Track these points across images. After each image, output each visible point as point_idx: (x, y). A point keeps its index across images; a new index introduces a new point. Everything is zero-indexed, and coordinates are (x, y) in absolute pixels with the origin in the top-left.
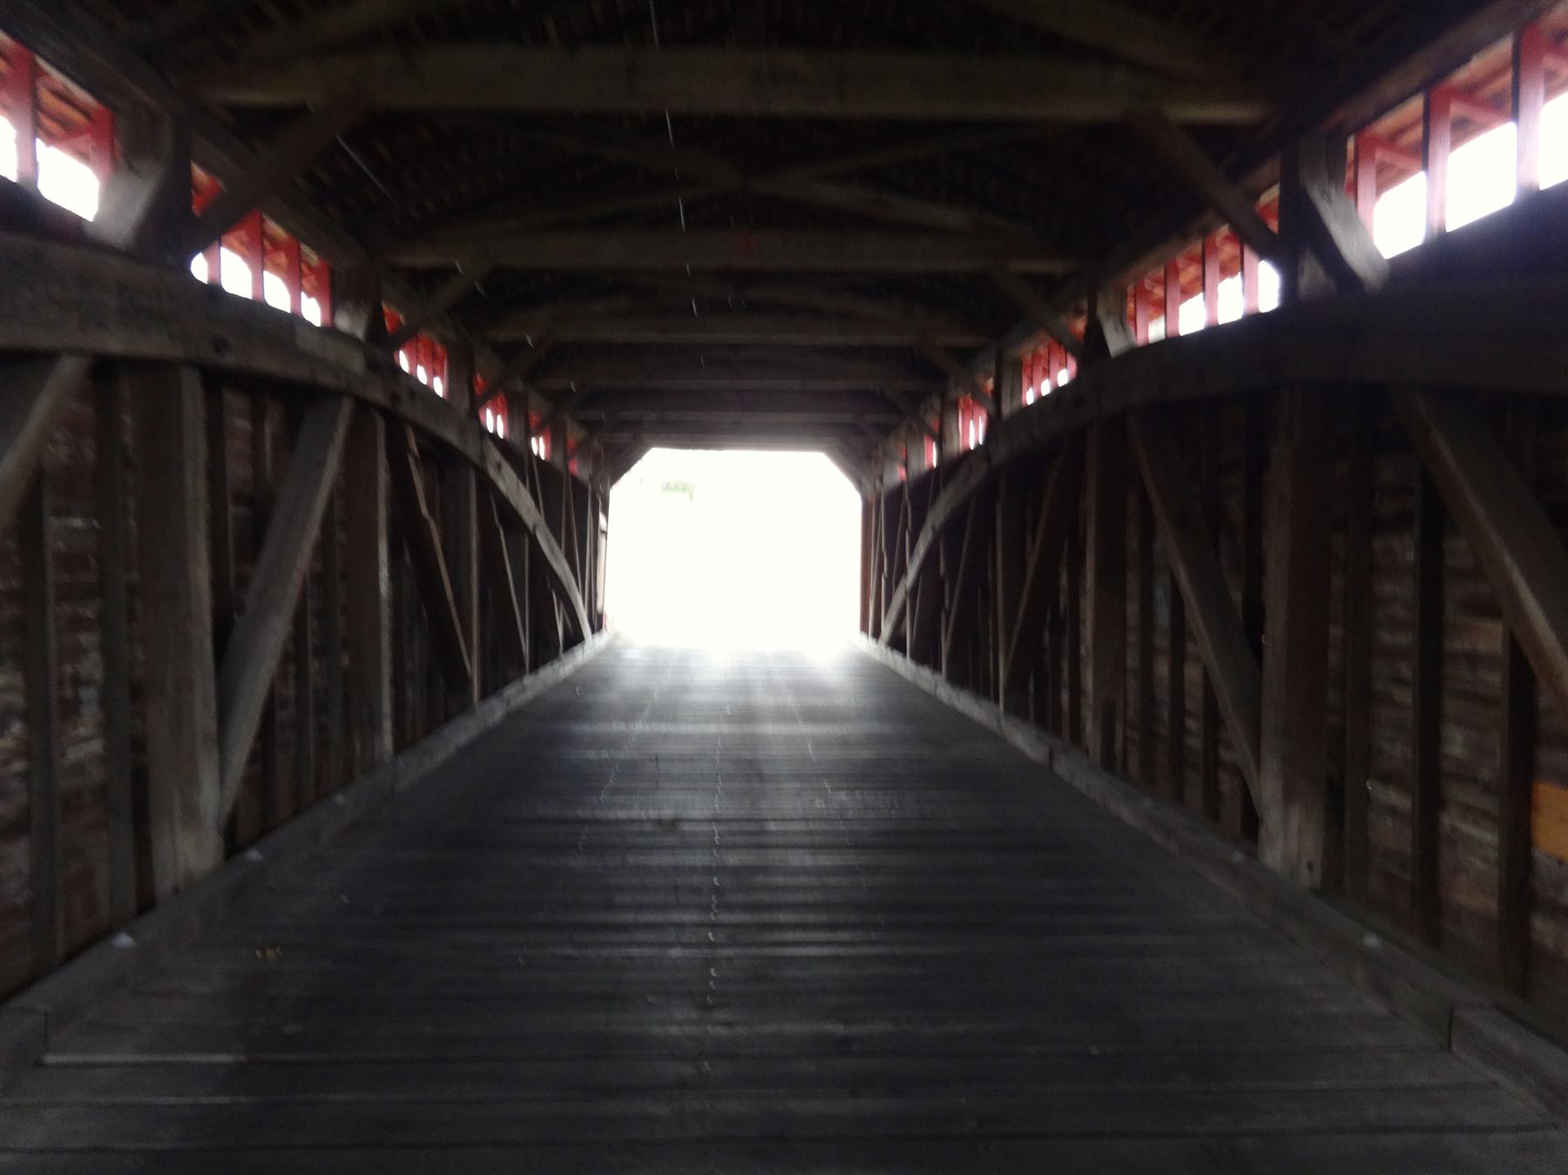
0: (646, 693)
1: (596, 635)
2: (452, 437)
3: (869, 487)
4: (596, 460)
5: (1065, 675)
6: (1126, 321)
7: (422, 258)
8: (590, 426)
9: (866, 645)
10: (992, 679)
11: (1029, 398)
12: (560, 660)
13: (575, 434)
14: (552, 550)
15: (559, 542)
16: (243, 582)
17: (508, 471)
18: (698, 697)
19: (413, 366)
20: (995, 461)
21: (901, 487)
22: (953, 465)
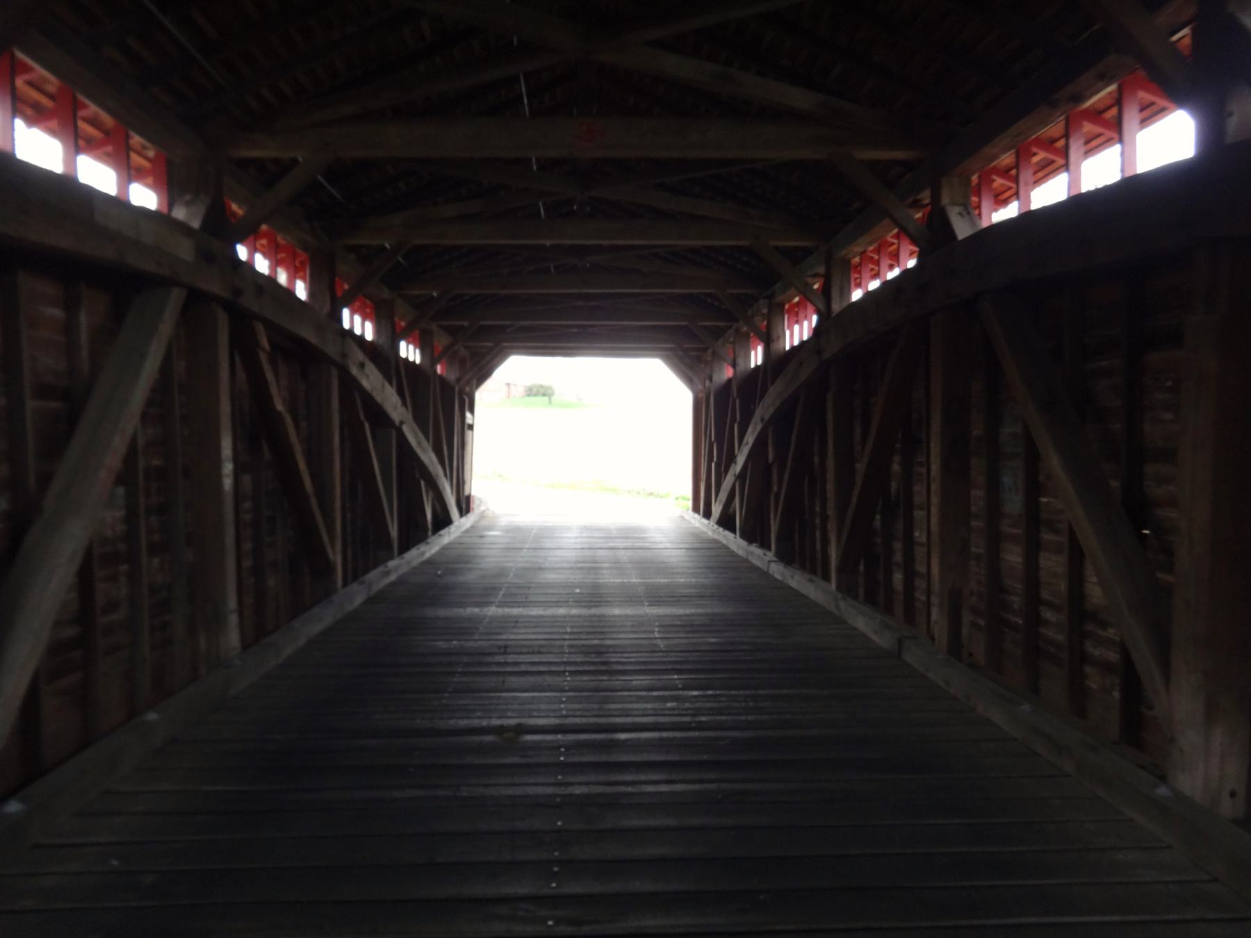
0: (502, 572)
2: (307, 333)
3: (700, 387)
4: (463, 362)
5: (898, 557)
6: (972, 211)
7: (264, 150)
8: (453, 332)
9: (697, 522)
10: (819, 555)
11: (857, 295)
12: (429, 540)
13: (441, 341)
14: (419, 444)
15: (427, 438)
16: (45, 480)
17: (371, 368)
18: (551, 577)
19: (292, 280)
20: (827, 355)
21: (730, 381)
22: (778, 363)
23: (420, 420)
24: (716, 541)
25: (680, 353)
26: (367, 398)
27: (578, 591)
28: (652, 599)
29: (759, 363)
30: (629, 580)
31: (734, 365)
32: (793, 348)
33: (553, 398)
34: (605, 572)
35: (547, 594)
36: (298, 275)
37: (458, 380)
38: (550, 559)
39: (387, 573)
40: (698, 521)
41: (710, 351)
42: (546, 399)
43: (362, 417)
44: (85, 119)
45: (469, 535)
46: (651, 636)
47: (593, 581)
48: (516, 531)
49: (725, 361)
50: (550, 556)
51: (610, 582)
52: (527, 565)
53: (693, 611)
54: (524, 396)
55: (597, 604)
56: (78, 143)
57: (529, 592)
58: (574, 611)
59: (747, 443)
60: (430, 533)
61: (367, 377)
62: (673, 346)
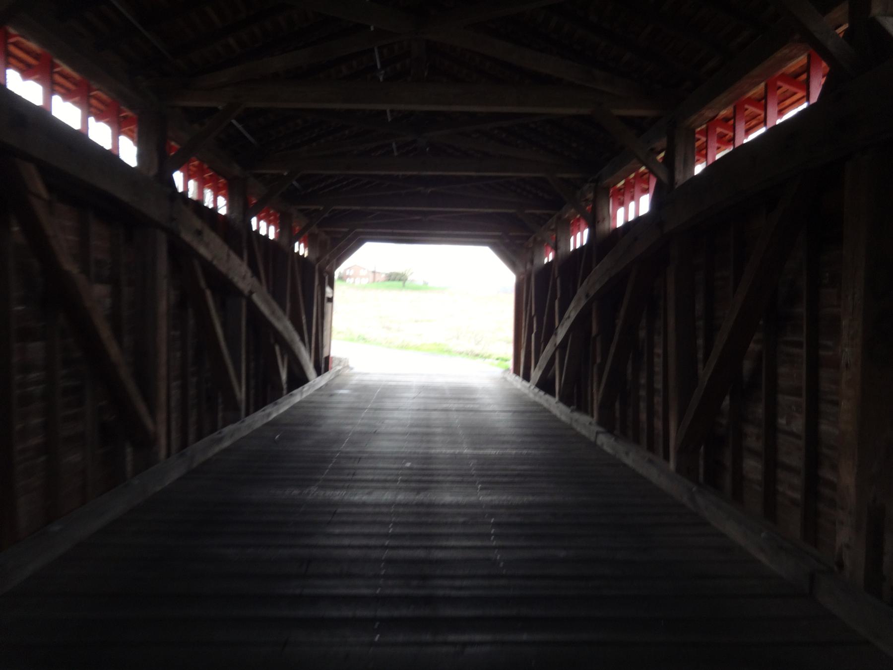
1: (320, 378)
11: (699, 169)
14: (273, 313)
18: (384, 445)
23: (277, 295)
24: (535, 404)
25: (507, 241)
26: (209, 269)
27: (408, 465)
28: (485, 479)
29: (585, 242)
30: (461, 451)
31: (556, 248)
32: (575, 250)
33: (407, 283)
34: (437, 438)
35: (376, 468)
36: (220, 192)
37: (318, 260)
38: (387, 421)
39: (220, 440)
40: (518, 383)
41: (531, 239)
42: (401, 283)
43: (203, 284)
44: (59, 73)
45: (322, 393)
46: (486, 543)
47: (426, 451)
48: (364, 390)
49: (548, 244)
50: (387, 419)
51: (441, 453)
52: (365, 429)
53: (531, 498)
54: (386, 281)
55: (425, 485)
56: (91, 109)
57: (359, 465)
58: (401, 497)
59: (569, 317)
60: (285, 392)
61: (207, 245)
62: (500, 234)
